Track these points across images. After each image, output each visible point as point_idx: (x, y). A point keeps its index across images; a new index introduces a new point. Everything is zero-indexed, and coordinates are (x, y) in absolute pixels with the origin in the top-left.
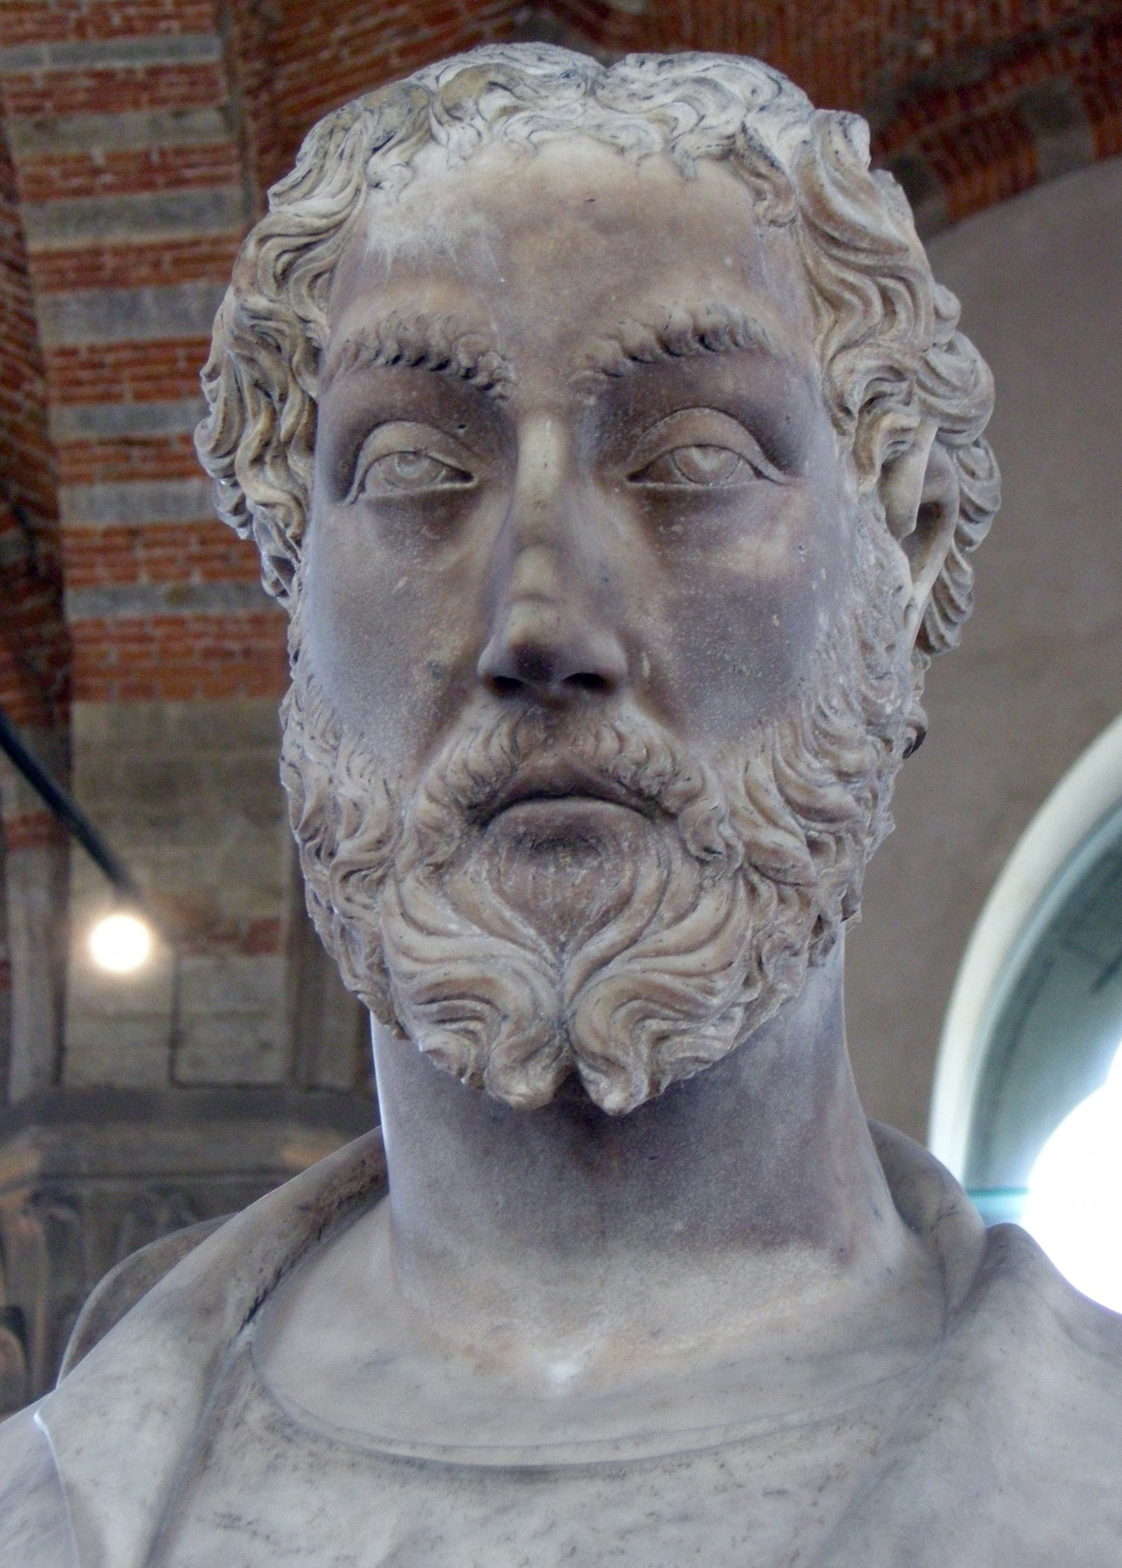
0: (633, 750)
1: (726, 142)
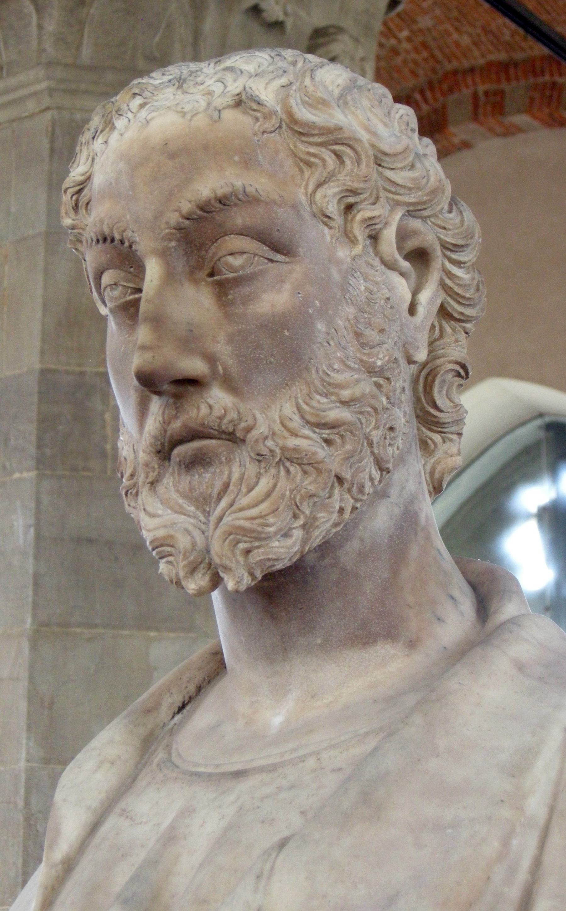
0: (217, 412)
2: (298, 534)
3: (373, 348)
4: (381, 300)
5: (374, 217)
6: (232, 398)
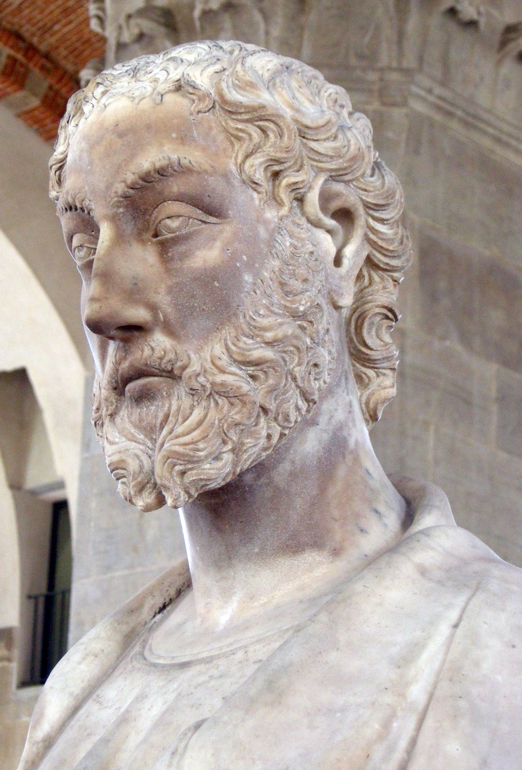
0: (158, 353)
1: (176, 83)
2: (228, 457)
3: (296, 295)
4: (305, 254)
5: (297, 183)
6: (171, 340)
